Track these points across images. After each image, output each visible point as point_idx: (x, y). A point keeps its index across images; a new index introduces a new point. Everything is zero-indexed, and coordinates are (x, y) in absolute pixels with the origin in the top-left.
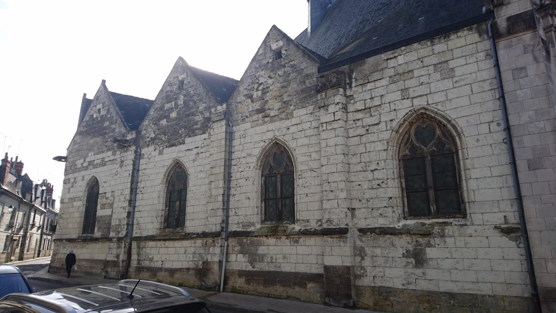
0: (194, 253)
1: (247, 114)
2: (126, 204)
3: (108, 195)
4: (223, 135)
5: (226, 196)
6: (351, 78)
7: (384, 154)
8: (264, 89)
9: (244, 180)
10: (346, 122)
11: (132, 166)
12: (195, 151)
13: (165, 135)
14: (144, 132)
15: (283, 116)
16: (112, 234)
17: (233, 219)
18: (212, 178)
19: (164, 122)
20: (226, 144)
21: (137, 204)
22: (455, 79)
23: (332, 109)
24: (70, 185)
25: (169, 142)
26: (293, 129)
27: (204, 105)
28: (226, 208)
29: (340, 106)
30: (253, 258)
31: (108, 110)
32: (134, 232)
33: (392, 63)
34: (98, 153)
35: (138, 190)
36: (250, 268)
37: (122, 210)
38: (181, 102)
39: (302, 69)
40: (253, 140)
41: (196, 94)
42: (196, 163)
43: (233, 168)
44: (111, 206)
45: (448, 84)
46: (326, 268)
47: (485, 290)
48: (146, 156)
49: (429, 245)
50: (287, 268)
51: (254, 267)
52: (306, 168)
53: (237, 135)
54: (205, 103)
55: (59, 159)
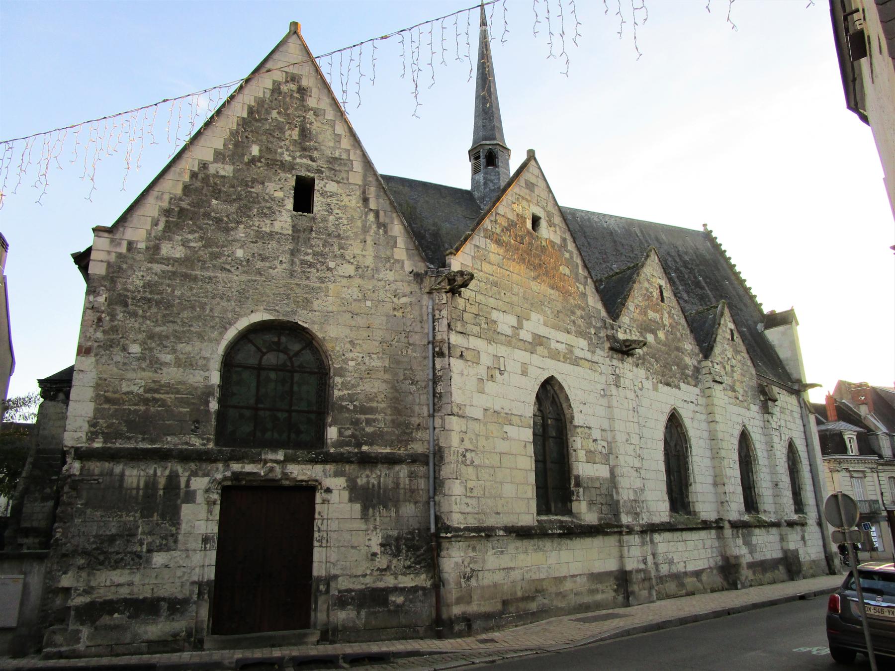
5: (551, 443)
16: (625, 519)
24: (482, 371)
30: (752, 549)
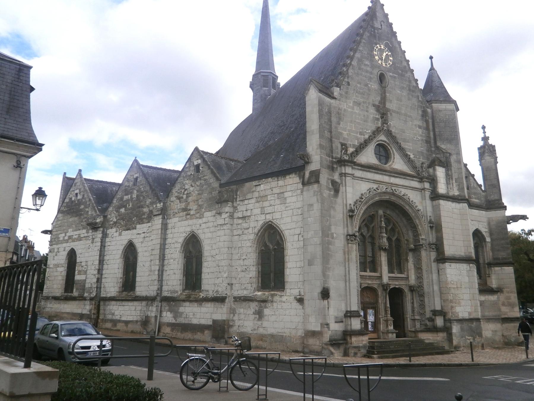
0: (141, 310)
1: (176, 211)
2: (96, 272)
3: (83, 264)
4: (160, 226)
5: (160, 271)
6: (237, 195)
7: (250, 249)
8: (187, 194)
9: (172, 260)
10: (232, 225)
11: (100, 243)
12: (143, 235)
13: (124, 220)
14: (109, 216)
15: (198, 215)
16: (86, 295)
17: (165, 288)
18: (152, 257)
19: (123, 210)
20: (161, 233)
21: (104, 272)
22: (287, 205)
23: (224, 216)
24: (55, 254)
25: (126, 226)
26: (204, 226)
27: (150, 200)
28: (161, 279)
29: (228, 214)
31: (83, 195)
32: (102, 293)
33: (258, 189)
34: (76, 230)
35: (104, 262)
36: (174, 321)
37: (93, 276)
38: (134, 196)
39: (211, 183)
40: (179, 229)
41: (145, 191)
42: (143, 245)
43: (166, 250)
44: (85, 273)
45: (283, 207)
46: (214, 321)
47: (287, 333)
48: (110, 236)
49: (266, 307)
50: (195, 321)
51: (176, 321)
52: (209, 254)
53: (170, 226)
54: (150, 199)
55: (45, 232)
